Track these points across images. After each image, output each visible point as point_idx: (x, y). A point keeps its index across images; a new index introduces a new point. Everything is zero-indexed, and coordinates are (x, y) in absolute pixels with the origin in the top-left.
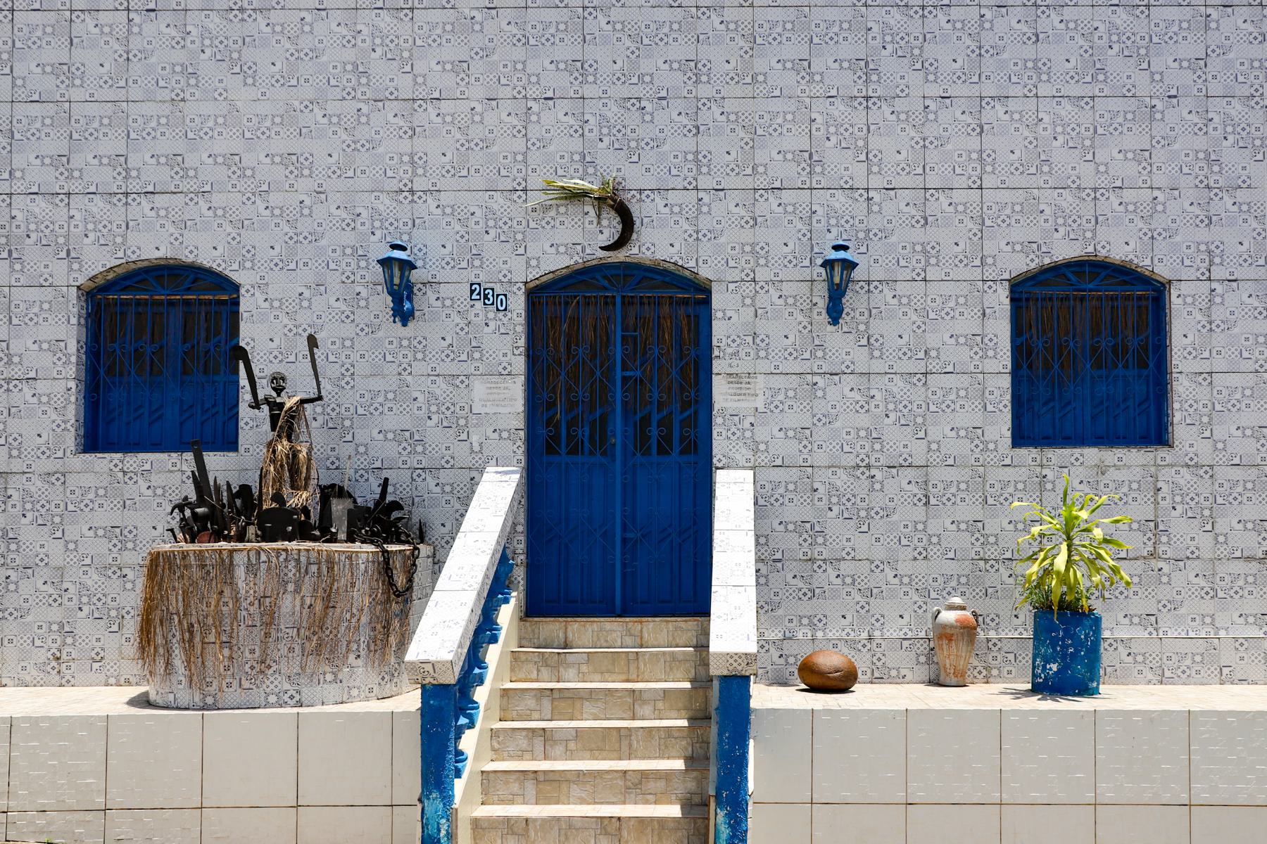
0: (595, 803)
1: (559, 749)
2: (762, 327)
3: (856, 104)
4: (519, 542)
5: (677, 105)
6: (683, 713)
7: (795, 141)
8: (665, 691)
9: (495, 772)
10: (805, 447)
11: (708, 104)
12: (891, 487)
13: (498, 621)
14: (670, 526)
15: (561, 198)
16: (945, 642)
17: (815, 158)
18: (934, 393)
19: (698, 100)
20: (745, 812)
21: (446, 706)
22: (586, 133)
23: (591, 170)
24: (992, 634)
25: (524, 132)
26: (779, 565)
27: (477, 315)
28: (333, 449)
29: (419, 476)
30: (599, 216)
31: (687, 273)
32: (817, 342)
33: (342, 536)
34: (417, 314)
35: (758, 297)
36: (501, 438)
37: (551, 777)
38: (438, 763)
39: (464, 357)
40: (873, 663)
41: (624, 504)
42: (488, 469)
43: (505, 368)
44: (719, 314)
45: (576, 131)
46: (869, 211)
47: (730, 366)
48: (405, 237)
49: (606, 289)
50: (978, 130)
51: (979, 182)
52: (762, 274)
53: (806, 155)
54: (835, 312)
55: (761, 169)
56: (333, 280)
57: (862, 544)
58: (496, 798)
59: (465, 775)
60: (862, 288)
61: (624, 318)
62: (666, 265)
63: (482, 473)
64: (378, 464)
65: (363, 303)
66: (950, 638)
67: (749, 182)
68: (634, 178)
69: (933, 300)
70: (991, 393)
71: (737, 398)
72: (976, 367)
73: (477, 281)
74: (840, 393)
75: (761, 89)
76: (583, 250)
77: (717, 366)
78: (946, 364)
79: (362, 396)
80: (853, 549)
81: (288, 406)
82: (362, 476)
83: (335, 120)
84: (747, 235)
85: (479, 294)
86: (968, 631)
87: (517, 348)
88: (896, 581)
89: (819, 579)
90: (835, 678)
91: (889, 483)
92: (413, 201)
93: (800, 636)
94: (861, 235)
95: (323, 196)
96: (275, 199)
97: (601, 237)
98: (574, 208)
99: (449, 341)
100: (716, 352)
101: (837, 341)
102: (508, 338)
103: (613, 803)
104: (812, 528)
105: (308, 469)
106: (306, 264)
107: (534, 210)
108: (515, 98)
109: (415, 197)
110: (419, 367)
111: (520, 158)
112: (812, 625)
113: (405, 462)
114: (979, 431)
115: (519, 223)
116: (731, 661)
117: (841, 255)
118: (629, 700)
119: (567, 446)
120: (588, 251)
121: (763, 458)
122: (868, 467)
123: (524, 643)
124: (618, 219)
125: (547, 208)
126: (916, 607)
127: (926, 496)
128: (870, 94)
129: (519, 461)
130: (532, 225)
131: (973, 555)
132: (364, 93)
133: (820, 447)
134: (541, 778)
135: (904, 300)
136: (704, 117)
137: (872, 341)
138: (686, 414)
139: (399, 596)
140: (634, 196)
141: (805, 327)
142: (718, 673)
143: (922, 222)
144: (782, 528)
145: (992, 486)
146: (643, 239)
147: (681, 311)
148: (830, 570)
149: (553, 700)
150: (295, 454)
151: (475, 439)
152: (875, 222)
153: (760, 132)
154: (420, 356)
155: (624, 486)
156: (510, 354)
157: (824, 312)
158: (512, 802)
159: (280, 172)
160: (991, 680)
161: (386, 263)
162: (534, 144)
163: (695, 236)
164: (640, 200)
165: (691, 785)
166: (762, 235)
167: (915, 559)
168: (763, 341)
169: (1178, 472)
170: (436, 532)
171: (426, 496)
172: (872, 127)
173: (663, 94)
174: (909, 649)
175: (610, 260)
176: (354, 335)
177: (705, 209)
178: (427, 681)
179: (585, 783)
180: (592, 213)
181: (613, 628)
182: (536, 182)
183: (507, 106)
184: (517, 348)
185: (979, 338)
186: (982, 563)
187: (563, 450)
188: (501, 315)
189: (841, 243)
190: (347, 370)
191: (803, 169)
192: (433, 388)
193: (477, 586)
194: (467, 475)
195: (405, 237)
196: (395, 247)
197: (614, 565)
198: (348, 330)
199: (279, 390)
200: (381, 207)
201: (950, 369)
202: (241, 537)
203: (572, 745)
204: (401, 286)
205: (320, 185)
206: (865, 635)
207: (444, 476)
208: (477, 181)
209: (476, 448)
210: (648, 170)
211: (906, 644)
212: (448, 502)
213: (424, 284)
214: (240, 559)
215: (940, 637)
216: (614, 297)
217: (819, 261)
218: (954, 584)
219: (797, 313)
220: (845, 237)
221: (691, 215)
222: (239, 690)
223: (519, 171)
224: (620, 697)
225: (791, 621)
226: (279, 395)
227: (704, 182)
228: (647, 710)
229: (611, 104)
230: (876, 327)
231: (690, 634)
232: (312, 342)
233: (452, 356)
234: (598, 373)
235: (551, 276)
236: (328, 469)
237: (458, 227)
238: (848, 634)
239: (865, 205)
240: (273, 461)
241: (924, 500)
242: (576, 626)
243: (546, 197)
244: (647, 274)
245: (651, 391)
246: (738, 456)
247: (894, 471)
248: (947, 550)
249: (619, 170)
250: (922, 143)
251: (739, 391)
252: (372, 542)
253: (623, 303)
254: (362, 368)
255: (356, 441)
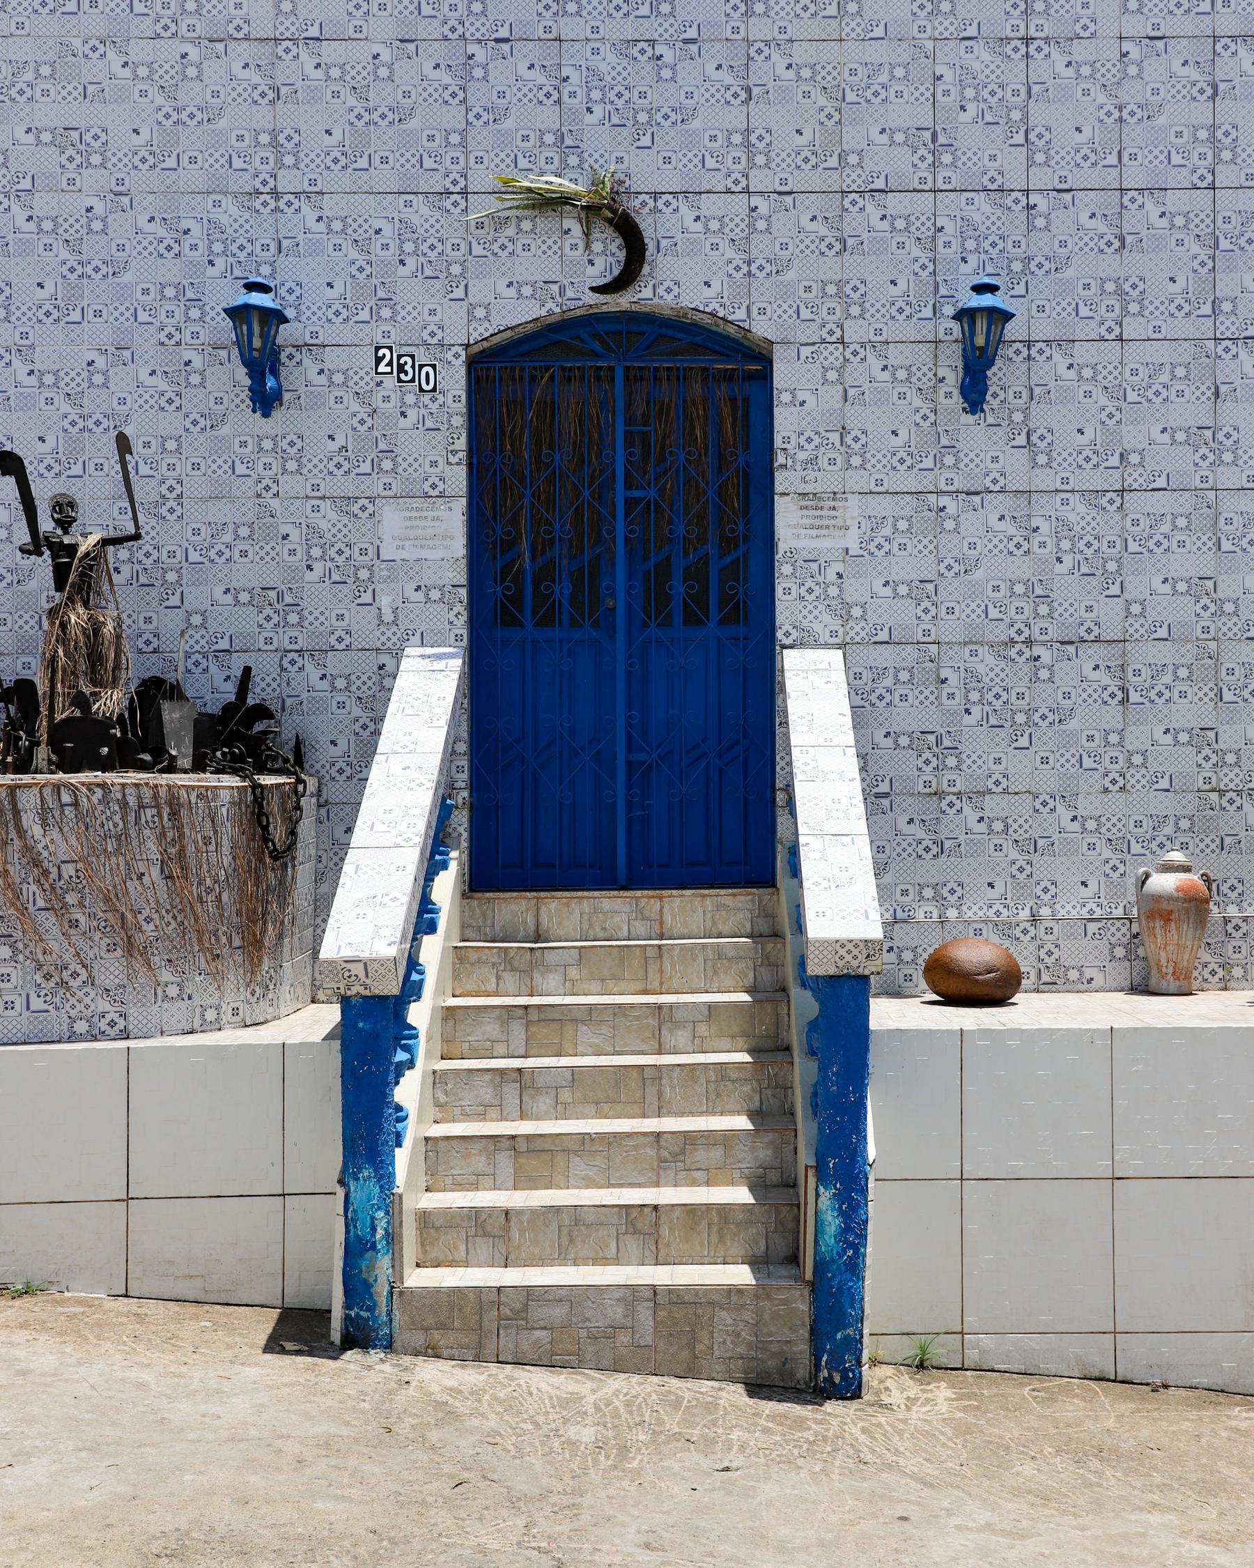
0: (610, 1186)
1: (544, 1102)
2: (857, 417)
3: (1008, 50)
4: (459, 769)
5: (718, 52)
6: (741, 1042)
7: (909, 112)
8: (710, 1007)
9: (448, 1138)
10: (926, 611)
11: (766, 51)
12: (1066, 675)
13: (433, 898)
14: (704, 740)
15: (526, 207)
16: (1159, 923)
17: (942, 139)
18: (1135, 522)
19: (750, 43)
20: (864, 1190)
21: (373, 1030)
22: (565, 98)
23: (573, 160)
24: (1232, 911)
25: (461, 95)
26: (886, 802)
27: (386, 399)
28: (148, 620)
29: (293, 662)
30: (587, 235)
31: (731, 330)
32: (944, 442)
33: (185, 762)
34: (286, 396)
35: (849, 368)
36: (428, 600)
37: (539, 1144)
38: (367, 1127)
39: (366, 468)
40: (1040, 960)
41: (629, 706)
42: (408, 651)
43: (434, 486)
44: (786, 397)
45: (548, 95)
46: (1031, 227)
47: (804, 480)
48: (266, 270)
49: (597, 355)
50: (1209, 91)
51: (1210, 178)
52: (856, 332)
53: (927, 135)
54: (974, 393)
55: (853, 159)
56: (145, 341)
57: (1020, 767)
58: (449, 1180)
59: (408, 1142)
60: (1018, 352)
61: (629, 404)
62: (698, 317)
63: (398, 656)
64: (224, 644)
65: (195, 379)
66: (1167, 917)
67: (834, 181)
68: (643, 172)
69: (1134, 372)
70: (1229, 521)
71: (814, 532)
72: (1204, 479)
73: (387, 342)
74: (982, 525)
75: (852, 27)
76: (562, 292)
77: (781, 481)
78: (1155, 475)
79: (196, 532)
80: (1006, 776)
81: (82, 550)
82: (197, 664)
83: (143, 71)
84: (830, 268)
85: (390, 364)
86: (1194, 907)
87: (454, 452)
88: (1076, 826)
89: (950, 826)
90: (986, 983)
91: (1062, 668)
92: (276, 210)
93: (920, 916)
94: (1017, 266)
95: (126, 200)
96: (43, 203)
97: (591, 271)
98: (546, 223)
99: (340, 441)
100: (780, 459)
101: (974, 433)
102: (439, 436)
103: (639, 1185)
104: (939, 741)
105: (117, 655)
106: (98, 313)
107: (480, 226)
108: (446, 39)
109: (282, 204)
110: (291, 485)
111: (455, 139)
112: (938, 898)
113: (269, 641)
114: (1210, 584)
115: (455, 247)
116: (842, 952)
117: (987, 300)
118: (653, 1022)
119: (534, 613)
120: (570, 293)
121: (857, 630)
122: (1029, 642)
123: (470, 933)
124: (619, 241)
125: (500, 223)
126: (1107, 869)
127: (1122, 689)
128: (1032, 32)
129: (458, 638)
130: (478, 250)
131: (921, 788)
132: (191, 28)
133: (950, 611)
134: (522, 1146)
135: (1087, 373)
136: (760, 71)
137: (1034, 438)
138: (728, 559)
139: (279, 860)
140: (644, 204)
141: (925, 418)
142: (820, 971)
143: (1117, 244)
144: (889, 742)
145: (1230, 672)
146: (660, 274)
147: (722, 391)
148: (967, 810)
149: (529, 1024)
150: (97, 628)
151: (385, 602)
152: (1041, 245)
153: (851, 97)
154: (292, 465)
155: (629, 674)
156: (441, 462)
157: (956, 392)
158: (475, 1187)
159: (50, 159)
160: (1231, 984)
161: (238, 313)
162: (478, 116)
163: (745, 269)
164: (655, 210)
165: (765, 1154)
166: (854, 267)
167: (1106, 790)
168: (856, 439)
169: (316, 509)
170: (323, 755)
171: (304, 695)
172: (1035, 89)
173: (692, 33)
174: (1097, 936)
175: (605, 309)
176: (181, 431)
177: (761, 225)
178: (354, 991)
179: (593, 1153)
180: (577, 230)
181: (614, 910)
182: (482, 179)
183: (438, 51)
184: (454, 452)
185: (1208, 433)
186: (1214, 796)
187: (528, 619)
188: (426, 398)
189: (987, 280)
190: (171, 489)
191: (922, 159)
192: (316, 519)
193: (419, 840)
194: (373, 660)
195: (266, 270)
196: (251, 287)
197: (613, 807)
198: (171, 423)
199: (65, 524)
200: (225, 220)
201: (1161, 483)
202: (23, 766)
203: (565, 1095)
204: (261, 346)
205: (120, 182)
206: (1025, 914)
207: (335, 663)
208: (385, 178)
209: (388, 616)
210: (666, 160)
211: (1092, 927)
212: (341, 705)
213: (298, 347)
214: (28, 800)
215: (1151, 916)
216: (611, 369)
217: (949, 310)
218: (1169, 830)
219: (912, 395)
220: (989, 269)
221: (738, 234)
222: (26, 1014)
223: (455, 161)
224: (637, 1018)
225: (905, 893)
226: (66, 532)
227: (760, 180)
228: (682, 1037)
229: (605, 49)
230: (1041, 417)
231: (740, 916)
232: (123, 445)
233: (346, 466)
234: (586, 494)
235: (509, 334)
236: (140, 652)
237: (353, 254)
238: (998, 914)
239: (1023, 216)
240: (63, 640)
241: (1120, 695)
242: (553, 905)
243: (500, 205)
244: (663, 331)
245: (670, 522)
246: (818, 628)
247: (1071, 649)
248: (1157, 777)
249: (620, 160)
250: (1116, 114)
251: (818, 522)
252: (234, 772)
253: (627, 378)
254: (196, 486)
255: (187, 606)
